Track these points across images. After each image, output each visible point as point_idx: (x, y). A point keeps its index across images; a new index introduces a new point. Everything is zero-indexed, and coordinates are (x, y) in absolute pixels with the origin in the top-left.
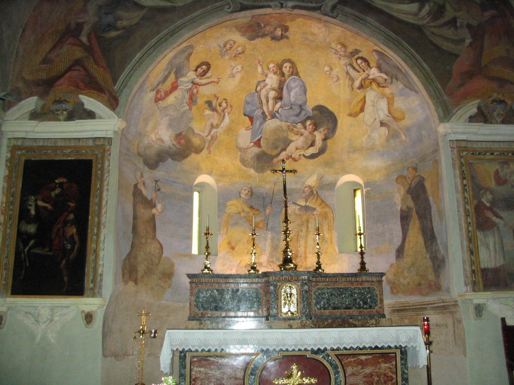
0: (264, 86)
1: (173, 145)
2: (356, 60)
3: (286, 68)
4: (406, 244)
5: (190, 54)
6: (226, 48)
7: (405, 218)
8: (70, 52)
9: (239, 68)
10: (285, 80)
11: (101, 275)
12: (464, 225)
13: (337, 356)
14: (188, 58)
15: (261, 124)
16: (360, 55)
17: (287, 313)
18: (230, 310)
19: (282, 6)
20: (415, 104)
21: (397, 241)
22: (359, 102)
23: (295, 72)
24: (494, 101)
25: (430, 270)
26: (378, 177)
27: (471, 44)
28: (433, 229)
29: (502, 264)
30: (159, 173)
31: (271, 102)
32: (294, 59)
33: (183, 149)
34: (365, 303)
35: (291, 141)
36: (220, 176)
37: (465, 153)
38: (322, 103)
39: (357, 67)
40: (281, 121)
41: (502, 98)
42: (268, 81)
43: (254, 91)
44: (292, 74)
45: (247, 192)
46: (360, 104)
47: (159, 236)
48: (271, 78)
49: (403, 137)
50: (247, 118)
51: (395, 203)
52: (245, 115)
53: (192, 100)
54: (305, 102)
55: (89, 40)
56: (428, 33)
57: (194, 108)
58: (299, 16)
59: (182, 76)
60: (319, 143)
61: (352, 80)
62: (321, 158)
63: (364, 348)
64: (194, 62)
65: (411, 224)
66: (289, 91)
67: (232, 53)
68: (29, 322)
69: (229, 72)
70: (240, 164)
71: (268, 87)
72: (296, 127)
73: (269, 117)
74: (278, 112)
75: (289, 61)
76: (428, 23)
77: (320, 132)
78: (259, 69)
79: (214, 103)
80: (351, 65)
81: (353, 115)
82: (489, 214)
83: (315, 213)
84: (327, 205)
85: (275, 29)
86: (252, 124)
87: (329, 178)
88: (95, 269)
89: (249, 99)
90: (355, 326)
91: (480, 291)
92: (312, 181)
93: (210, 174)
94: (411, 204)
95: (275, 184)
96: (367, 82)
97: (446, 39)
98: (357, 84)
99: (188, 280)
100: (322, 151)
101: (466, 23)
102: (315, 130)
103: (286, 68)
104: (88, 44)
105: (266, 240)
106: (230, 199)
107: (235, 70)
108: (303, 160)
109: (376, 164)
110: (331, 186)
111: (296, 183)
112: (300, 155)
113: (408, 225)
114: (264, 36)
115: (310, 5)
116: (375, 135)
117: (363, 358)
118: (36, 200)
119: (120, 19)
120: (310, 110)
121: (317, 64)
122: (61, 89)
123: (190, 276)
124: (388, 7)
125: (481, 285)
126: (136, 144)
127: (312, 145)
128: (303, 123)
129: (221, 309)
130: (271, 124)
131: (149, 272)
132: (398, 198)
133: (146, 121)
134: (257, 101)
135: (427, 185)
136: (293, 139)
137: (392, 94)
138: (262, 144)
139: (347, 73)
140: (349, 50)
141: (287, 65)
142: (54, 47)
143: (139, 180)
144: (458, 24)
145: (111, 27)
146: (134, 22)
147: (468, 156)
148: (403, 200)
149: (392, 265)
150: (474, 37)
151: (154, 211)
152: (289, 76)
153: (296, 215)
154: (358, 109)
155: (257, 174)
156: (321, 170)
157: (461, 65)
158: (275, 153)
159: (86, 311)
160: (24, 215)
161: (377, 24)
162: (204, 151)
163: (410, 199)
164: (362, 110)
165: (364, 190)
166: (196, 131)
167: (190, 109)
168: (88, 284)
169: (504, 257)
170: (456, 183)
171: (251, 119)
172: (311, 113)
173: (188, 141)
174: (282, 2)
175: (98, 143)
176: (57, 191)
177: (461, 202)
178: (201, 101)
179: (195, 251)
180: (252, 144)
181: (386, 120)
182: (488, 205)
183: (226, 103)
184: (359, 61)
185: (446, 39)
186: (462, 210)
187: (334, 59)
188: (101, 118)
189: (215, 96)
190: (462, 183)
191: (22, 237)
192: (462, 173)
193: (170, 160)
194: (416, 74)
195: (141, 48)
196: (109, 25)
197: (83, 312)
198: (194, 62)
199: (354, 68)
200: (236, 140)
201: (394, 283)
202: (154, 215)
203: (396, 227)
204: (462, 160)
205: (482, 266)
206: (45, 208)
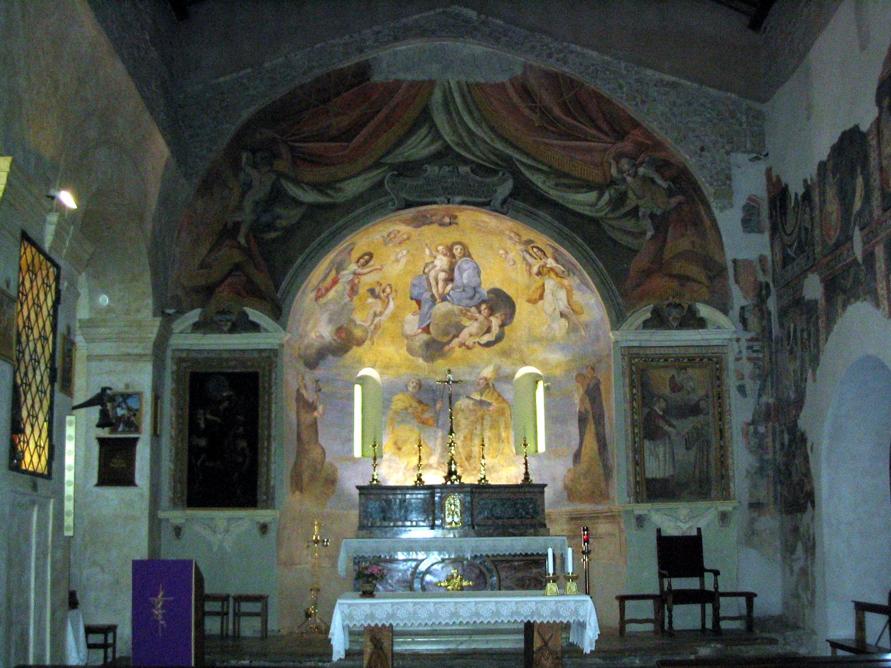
2: (532, 248)
3: (457, 250)
5: (352, 250)
6: (388, 240)
7: (582, 421)
8: (229, 255)
9: (405, 252)
11: (274, 487)
12: (630, 436)
13: (493, 562)
14: (349, 254)
17: (451, 523)
18: (397, 520)
19: (449, 202)
20: (592, 304)
22: (537, 289)
23: (466, 254)
24: (669, 305)
25: (602, 478)
26: (558, 372)
27: (653, 237)
29: (672, 473)
30: (319, 373)
31: (441, 284)
32: (465, 240)
33: (345, 342)
34: (527, 513)
35: (465, 327)
36: (385, 368)
37: (636, 360)
38: (498, 285)
40: (453, 304)
41: (677, 301)
42: (438, 263)
43: (421, 273)
44: (464, 256)
46: (539, 291)
47: (321, 441)
49: (583, 333)
50: (414, 302)
51: (574, 404)
52: (412, 299)
54: (480, 285)
55: (247, 241)
56: (606, 227)
57: (355, 298)
59: (344, 269)
60: (495, 330)
61: (530, 266)
62: (497, 347)
63: (515, 555)
64: (355, 255)
65: (588, 426)
67: (397, 240)
68: (206, 533)
69: (393, 258)
71: (438, 268)
72: (469, 311)
73: (438, 300)
74: (448, 294)
75: (460, 243)
76: (606, 214)
78: (427, 252)
79: (377, 290)
80: (527, 252)
81: (533, 302)
82: (661, 423)
83: (491, 408)
84: (504, 400)
87: (507, 368)
88: (268, 481)
89: (416, 282)
90: (514, 535)
91: (642, 502)
92: (487, 372)
93: (373, 367)
94: (588, 406)
97: (627, 232)
98: (535, 269)
99: (358, 491)
100: (499, 338)
101: (649, 212)
104: (246, 245)
105: (436, 439)
106: (396, 394)
108: (478, 349)
109: (556, 357)
110: (508, 378)
111: (471, 374)
112: (474, 343)
113: (585, 427)
114: (431, 223)
116: (555, 325)
117: (516, 564)
118: (205, 414)
119: (279, 217)
121: (491, 247)
122: (223, 294)
123: (358, 487)
124: (562, 198)
125: (645, 496)
126: (297, 347)
127: (488, 330)
128: (478, 307)
129: (390, 519)
130: (442, 307)
131: (313, 478)
133: (307, 321)
134: (425, 284)
135: (602, 388)
136: (467, 324)
139: (524, 258)
142: (211, 250)
143: (301, 384)
144: (640, 214)
145: (270, 227)
146: (294, 221)
148: (582, 401)
150: (656, 229)
151: (316, 414)
152: (461, 258)
153: (470, 411)
154: (537, 296)
155: (426, 364)
156: (497, 360)
157: (641, 261)
158: (445, 340)
159: (262, 521)
160: (193, 429)
161: (549, 218)
163: (587, 401)
164: (541, 297)
166: (358, 323)
168: (262, 497)
169: (674, 467)
170: (625, 393)
171: (419, 303)
173: (350, 333)
175: (264, 354)
176: (226, 404)
177: (629, 414)
178: (362, 290)
179: (357, 453)
180: (420, 330)
181: (567, 310)
182: (661, 413)
183: (391, 288)
184: (535, 250)
185: (627, 232)
186: (629, 420)
187: (509, 243)
188: (266, 331)
189: (378, 283)
190: (631, 391)
191: (193, 451)
192: (632, 381)
193: (330, 357)
194: (589, 274)
195: (301, 251)
196: (268, 226)
197: (258, 522)
198: (355, 255)
200: (403, 327)
201: (571, 490)
202: (315, 419)
205: (649, 475)
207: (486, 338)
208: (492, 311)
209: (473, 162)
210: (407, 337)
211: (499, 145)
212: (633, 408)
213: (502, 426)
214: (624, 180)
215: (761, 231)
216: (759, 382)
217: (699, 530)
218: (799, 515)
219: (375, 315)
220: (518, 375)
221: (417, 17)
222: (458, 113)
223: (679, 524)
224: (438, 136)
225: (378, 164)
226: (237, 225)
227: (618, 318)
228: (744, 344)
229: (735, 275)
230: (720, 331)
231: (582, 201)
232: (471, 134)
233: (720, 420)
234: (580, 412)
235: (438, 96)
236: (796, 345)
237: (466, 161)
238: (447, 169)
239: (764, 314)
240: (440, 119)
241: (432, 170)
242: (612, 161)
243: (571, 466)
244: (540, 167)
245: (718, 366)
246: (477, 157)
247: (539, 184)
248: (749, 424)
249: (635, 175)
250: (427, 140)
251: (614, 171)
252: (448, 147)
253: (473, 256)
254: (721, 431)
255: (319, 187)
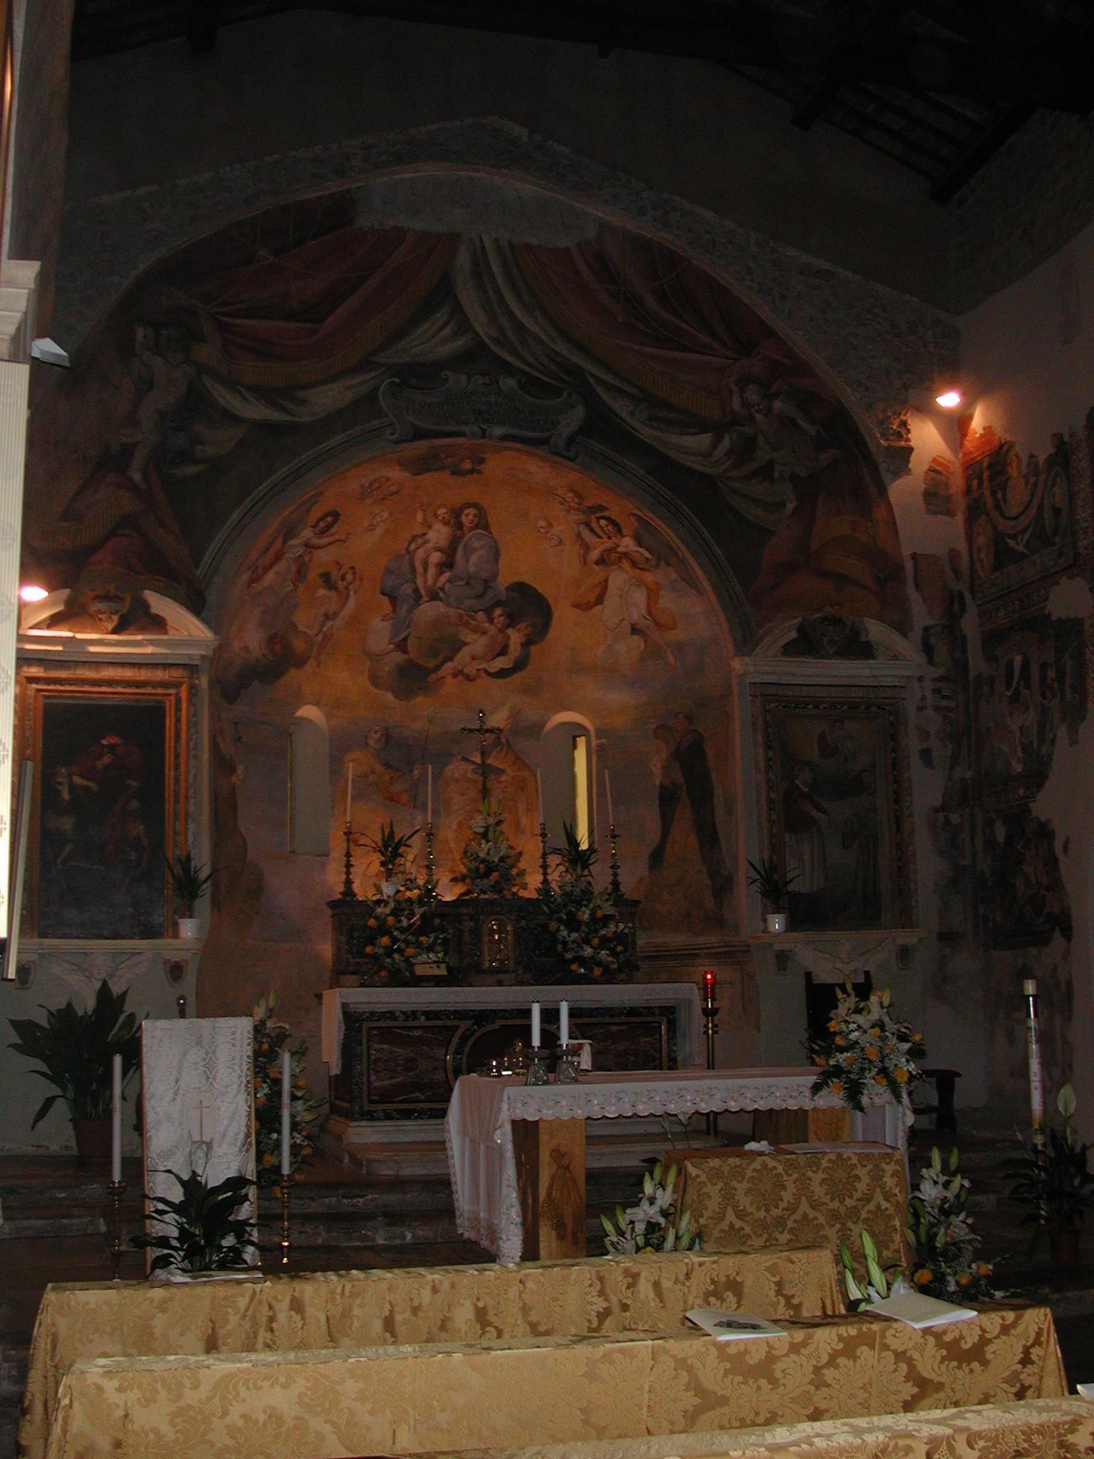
0: (423, 544)
1: (264, 656)
2: (598, 519)
3: (468, 517)
4: (668, 846)
7: (667, 800)
9: (385, 515)
10: (463, 535)
14: (309, 510)
15: (410, 611)
16: (606, 514)
20: (695, 614)
21: (653, 838)
23: (482, 523)
24: (824, 619)
28: (714, 824)
31: (432, 571)
37: (773, 705)
38: (526, 579)
39: (598, 530)
40: (448, 605)
43: (403, 552)
44: (477, 527)
45: (379, 735)
46: (597, 591)
48: (438, 531)
49: (671, 659)
53: (300, 574)
54: (495, 576)
58: (507, 449)
59: (294, 537)
61: (587, 548)
64: (315, 514)
66: (468, 552)
69: (366, 523)
70: (368, 683)
73: (425, 598)
75: (474, 505)
77: (519, 631)
78: (419, 516)
79: (335, 574)
80: (588, 525)
81: (584, 607)
83: (503, 778)
84: (526, 766)
85: (462, 461)
86: (394, 611)
94: (680, 778)
95: (430, 722)
96: (613, 556)
98: (595, 555)
100: (520, 665)
102: (509, 626)
103: (468, 517)
107: (378, 518)
108: (484, 681)
109: (619, 700)
110: (535, 730)
115: (531, 434)
117: (614, 1028)
118: (70, 775)
120: (502, 589)
128: (488, 612)
130: (429, 610)
132: (657, 763)
136: (468, 640)
137: (656, 583)
138: (410, 648)
139: (579, 536)
140: (588, 503)
141: (472, 511)
144: (776, 474)
147: (779, 710)
149: (641, 880)
154: (592, 598)
158: (431, 664)
162: (308, 665)
164: (600, 600)
165: (594, 743)
166: (301, 628)
167: (296, 587)
171: (393, 600)
172: (503, 595)
174: (484, 426)
178: (313, 575)
182: (806, 790)
183: (354, 573)
184: (603, 522)
189: (338, 563)
193: (256, 684)
197: (167, 961)
199: (592, 531)
203: (650, 816)
204: (768, 717)
206: (86, 788)
207: (500, 663)
208: (512, 621)
209: (523, 372)
210: (369, 655)
211: (562, 348)
212: (769, 780)
213: (522, 807)
214: (752, 418)
215: (951, 513)
216: (951, 746)
217: (867, 973)
218: (1032, 951)
219: (327, 617)
220: (549, 726)
221: (433, 127)
222: (498, 291)
223: (840, 965)
224: (464, 326)
225: (365, 365)
226: (128, 451)
227: (746, 641)
228: (928, 685)
229: (915, 577)
230: (896, 661)
231: (690, 446)
232: (519, 327)
233: (896, 802)
234: (661, 786)
235: (463, 259)
236: (1028, 686)
237: (509, 370)
238: (481, 380)
239: (957, 640)
240: (468, 298)
241: (457, 381)
242: (735, 389)
243: (646, 873)
244: (627, 388)
245: (892, 718)
246: (528, 364)
247: (624, 415)
248: (937, 810)
249: (768, 412)
250: (447, 331)
251: (736, 404)
252: (482, 345)
253: (492, 529)
254: (898, 820)
255: (264, 394)
